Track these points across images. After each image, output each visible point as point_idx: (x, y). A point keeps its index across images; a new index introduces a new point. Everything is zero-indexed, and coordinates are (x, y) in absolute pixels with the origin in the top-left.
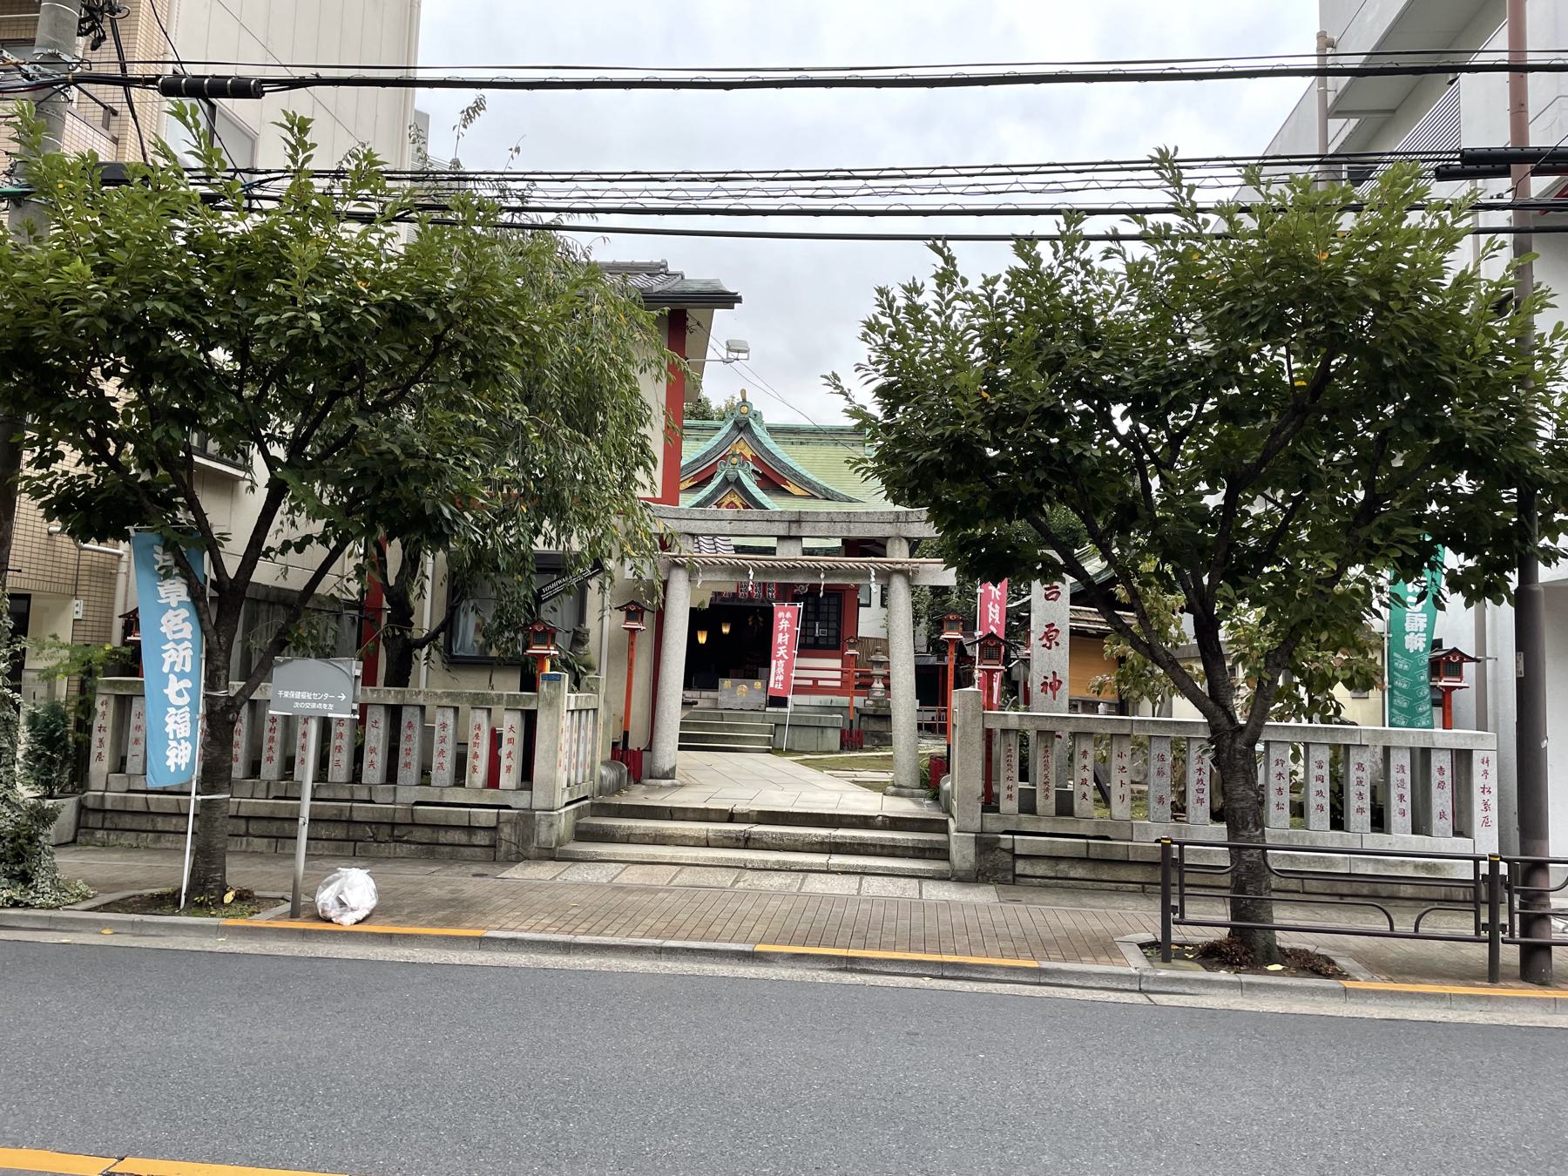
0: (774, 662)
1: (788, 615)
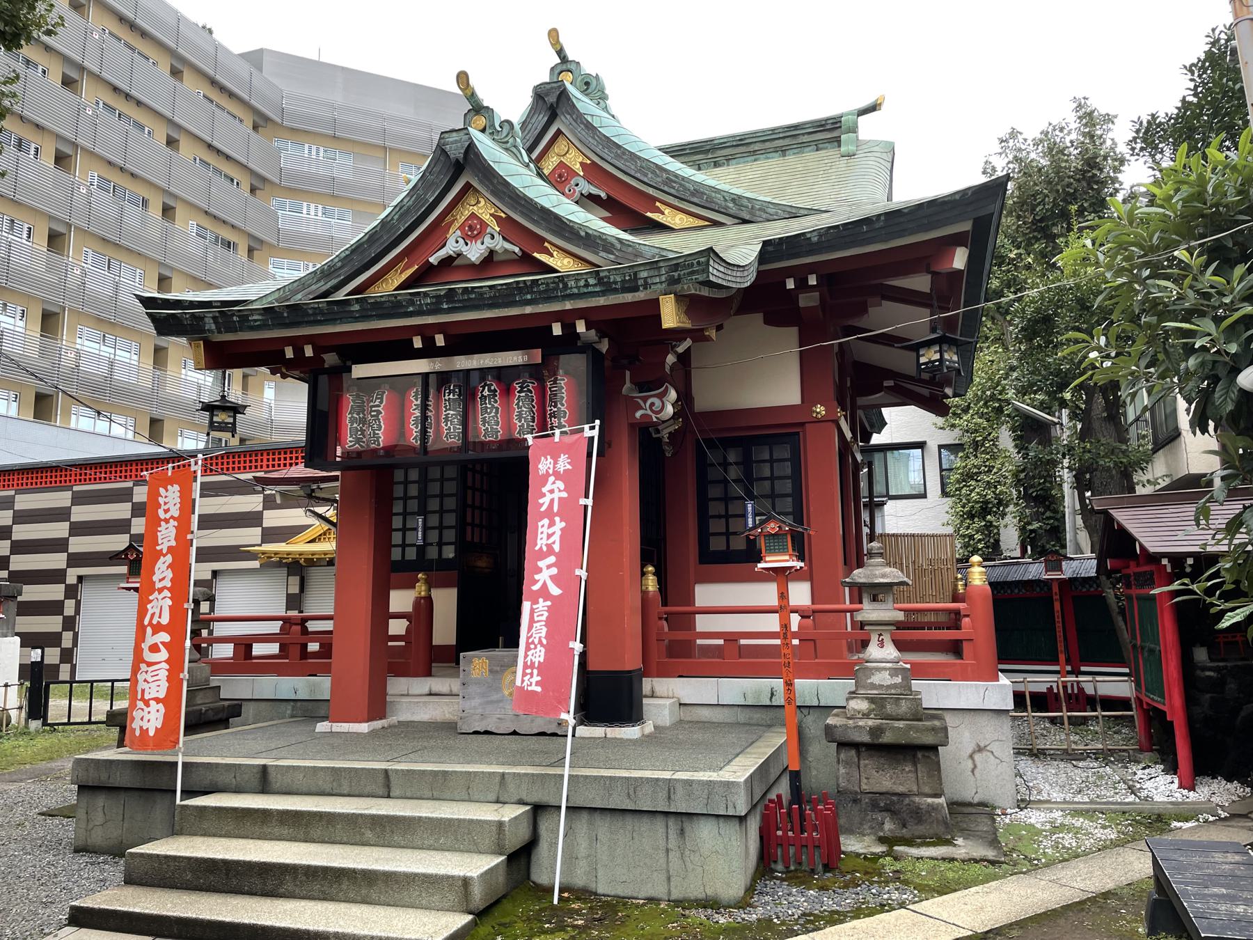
0: (526, 606)
1: (564, 464)
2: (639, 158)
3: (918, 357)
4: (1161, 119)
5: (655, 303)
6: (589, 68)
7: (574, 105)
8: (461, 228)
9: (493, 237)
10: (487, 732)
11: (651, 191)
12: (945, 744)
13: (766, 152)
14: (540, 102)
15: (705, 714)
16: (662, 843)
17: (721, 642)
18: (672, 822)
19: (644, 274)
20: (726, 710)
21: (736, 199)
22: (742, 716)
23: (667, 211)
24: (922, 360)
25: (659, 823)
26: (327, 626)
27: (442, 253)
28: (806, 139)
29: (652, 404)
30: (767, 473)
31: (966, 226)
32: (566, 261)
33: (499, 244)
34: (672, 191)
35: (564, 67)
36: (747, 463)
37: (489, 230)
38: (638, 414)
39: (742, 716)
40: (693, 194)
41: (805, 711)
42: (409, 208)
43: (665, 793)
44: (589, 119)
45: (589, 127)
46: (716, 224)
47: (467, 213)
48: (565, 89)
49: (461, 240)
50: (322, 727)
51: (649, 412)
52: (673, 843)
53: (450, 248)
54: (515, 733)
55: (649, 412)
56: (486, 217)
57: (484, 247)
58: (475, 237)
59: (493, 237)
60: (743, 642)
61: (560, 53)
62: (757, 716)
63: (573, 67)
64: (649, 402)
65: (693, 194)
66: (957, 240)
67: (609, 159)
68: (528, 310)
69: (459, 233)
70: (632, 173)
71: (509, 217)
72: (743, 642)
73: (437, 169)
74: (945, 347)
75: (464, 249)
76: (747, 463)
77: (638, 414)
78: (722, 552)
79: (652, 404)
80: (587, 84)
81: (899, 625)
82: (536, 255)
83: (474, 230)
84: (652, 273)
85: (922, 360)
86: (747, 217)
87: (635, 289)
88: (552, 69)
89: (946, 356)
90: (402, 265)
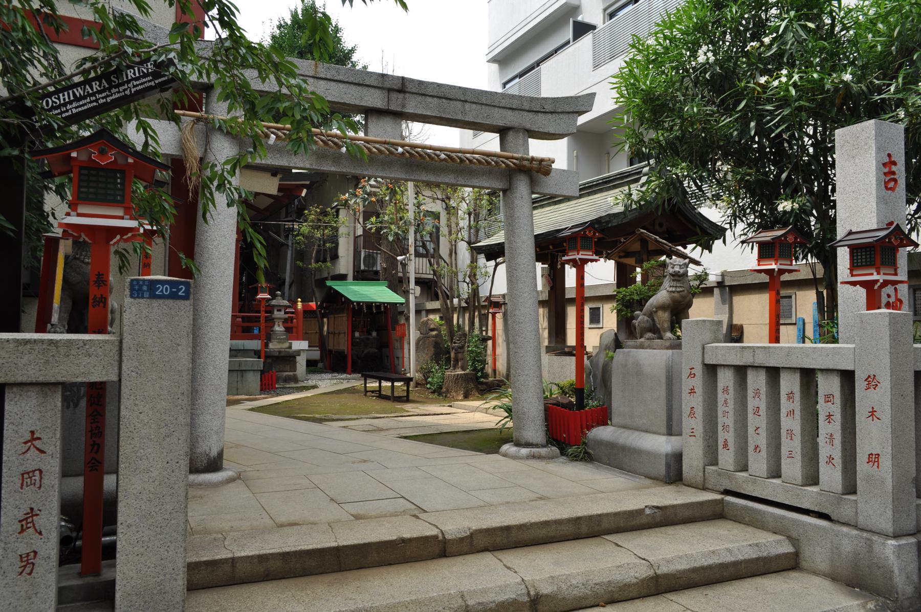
31: (308, 183)
52: (239, 379)
66: (304, 186)
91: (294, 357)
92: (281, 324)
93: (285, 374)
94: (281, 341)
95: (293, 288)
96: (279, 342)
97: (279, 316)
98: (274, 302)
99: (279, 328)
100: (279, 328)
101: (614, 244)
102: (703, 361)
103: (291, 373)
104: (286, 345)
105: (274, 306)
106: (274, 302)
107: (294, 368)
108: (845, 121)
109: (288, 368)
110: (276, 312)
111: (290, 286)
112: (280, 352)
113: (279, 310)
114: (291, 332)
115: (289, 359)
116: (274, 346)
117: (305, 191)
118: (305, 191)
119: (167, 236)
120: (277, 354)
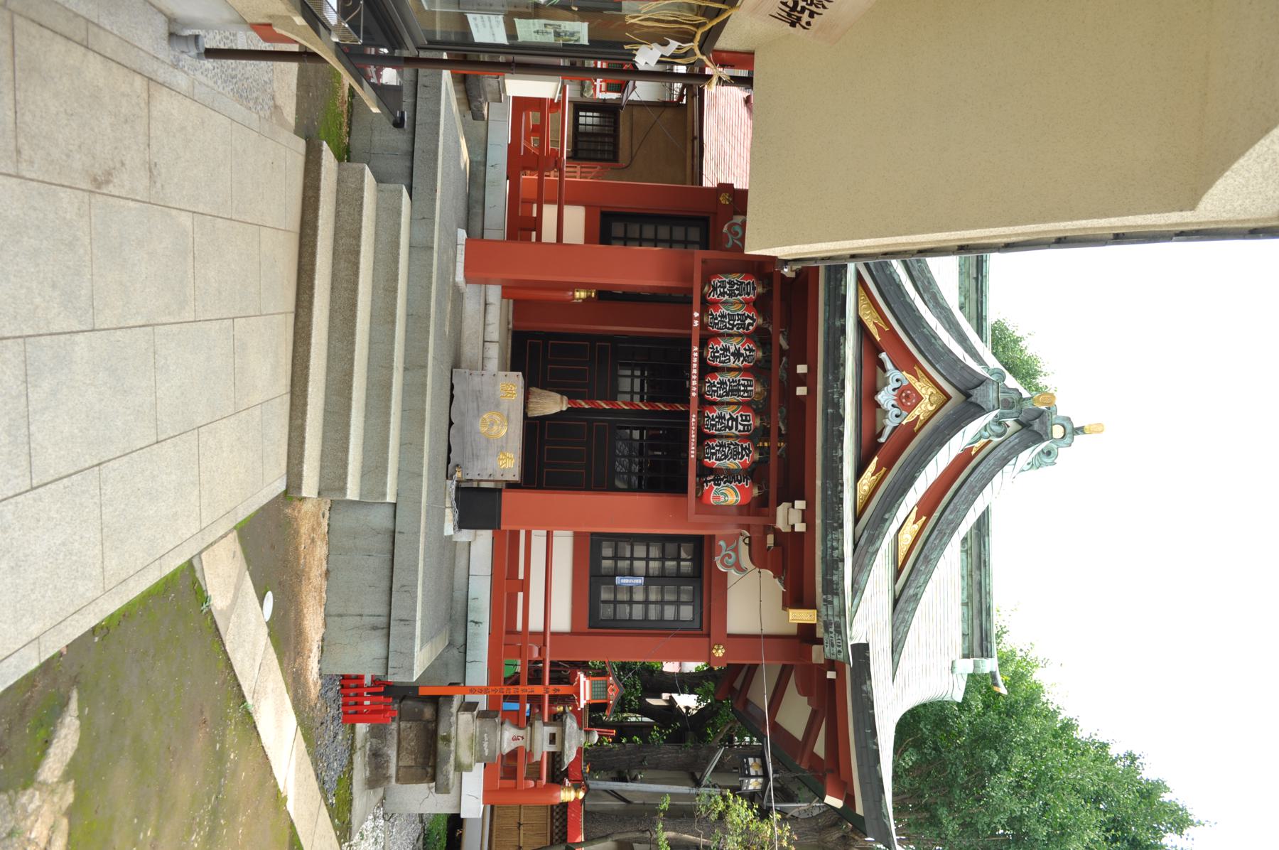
2: (968, 509)
3: (755, 757)
4: (1050, 706)
5: (812, 605)
6: (1063, 453)
7: (1027, 447)
8: (910, 387)
9: (897, 416)
10: (452, 397)
11: (936, 514)
12: (437, 790)
13: (969, 586)
14: (1036, 414)
15: (461, 562)
16: (367, 611)
17: (521, 576)
18: (384, 620)
19: (836, 601)
20: (464, 580)
21: (916, 598)
22: (459, 595)
23: (917, 527)
24: (751, 760)
25: (382, 610)
26: (549, 234)
27: (889, 365)
28: (976, 622)
29: (730, 556)
30: (668, 597)
31: (859, 810)
32: (866, 488)
33: (891, 423)
34: (933, 536)
35: (1069, 430)
36: (679, 578)
37: (905, 413)
38: (722, 543)
39: (459, 595)
40: (926, 557)
41: (462, 649)
42: (932, 344)
43: (405, 617)
44: (1013, 462)
45: (1004, 462)
46: (898, 572)
47: (922, 392)
48: (1044, 440)
49: (897, 385)
50: (462, 234)
51: (724, 553)
52: (367, 620)
53: (893, 374)
54: (451, 424)
55: (724, 553)
56: (916, 412)
57: (889, 407)
58: (899, 398)
59: (897, 416)
60: (520, 595)
61: (1080, 430)
62: (459, 607)
63: (1067, 440)
64: (733, 554)
65: (926, 557)
66: (849, 800)
67: (971, 479)
68: (819, 483)
69: (905, 383)
70: (955, 501)
71: (914, 435)
72: (520, 595)
73: (966, 375)
74: (760, 780)
75: (890, 387)
76: (679, 578)
77: (722, 543)
78: (600, 551)
79: (730, 556)
80: (1049, 453)
81: (530, 754)
82: (876, 459)
83: (907, 397)
84: (837, 609)
85: (751, 760)
86: (899, 607)
87: (824, 592)
88: (1069, 419)
89: (752, 780)
90: (882, 324)
91: (434, 779)
92: (520, 743)
93: (392, 753)
94: (476, 742)
95: (616, 804)
96: (472, 738)
97: (538, 736)
98: (571, 724)
99: (509, 738)
100: (509, 738)
101: (698, 685)
102: (525, 414)
103: (392, 770)
104: (465, 757)
105: (563, 725)
106: (571, 724)
107: (407, 777)
108: (838, 540)
109: (408, 761)
110: (549, 730)
111: (614, 794)
112: (447, 739)
113: (553, 739)
114: (507, 769)
115: (429, 762)
116: (462, 728)
117: (837, 803)
118: (837, 803)
119: (723, 7)
120: (442, 732)
